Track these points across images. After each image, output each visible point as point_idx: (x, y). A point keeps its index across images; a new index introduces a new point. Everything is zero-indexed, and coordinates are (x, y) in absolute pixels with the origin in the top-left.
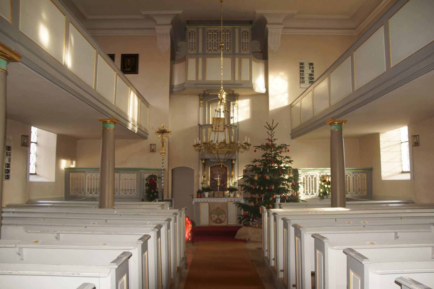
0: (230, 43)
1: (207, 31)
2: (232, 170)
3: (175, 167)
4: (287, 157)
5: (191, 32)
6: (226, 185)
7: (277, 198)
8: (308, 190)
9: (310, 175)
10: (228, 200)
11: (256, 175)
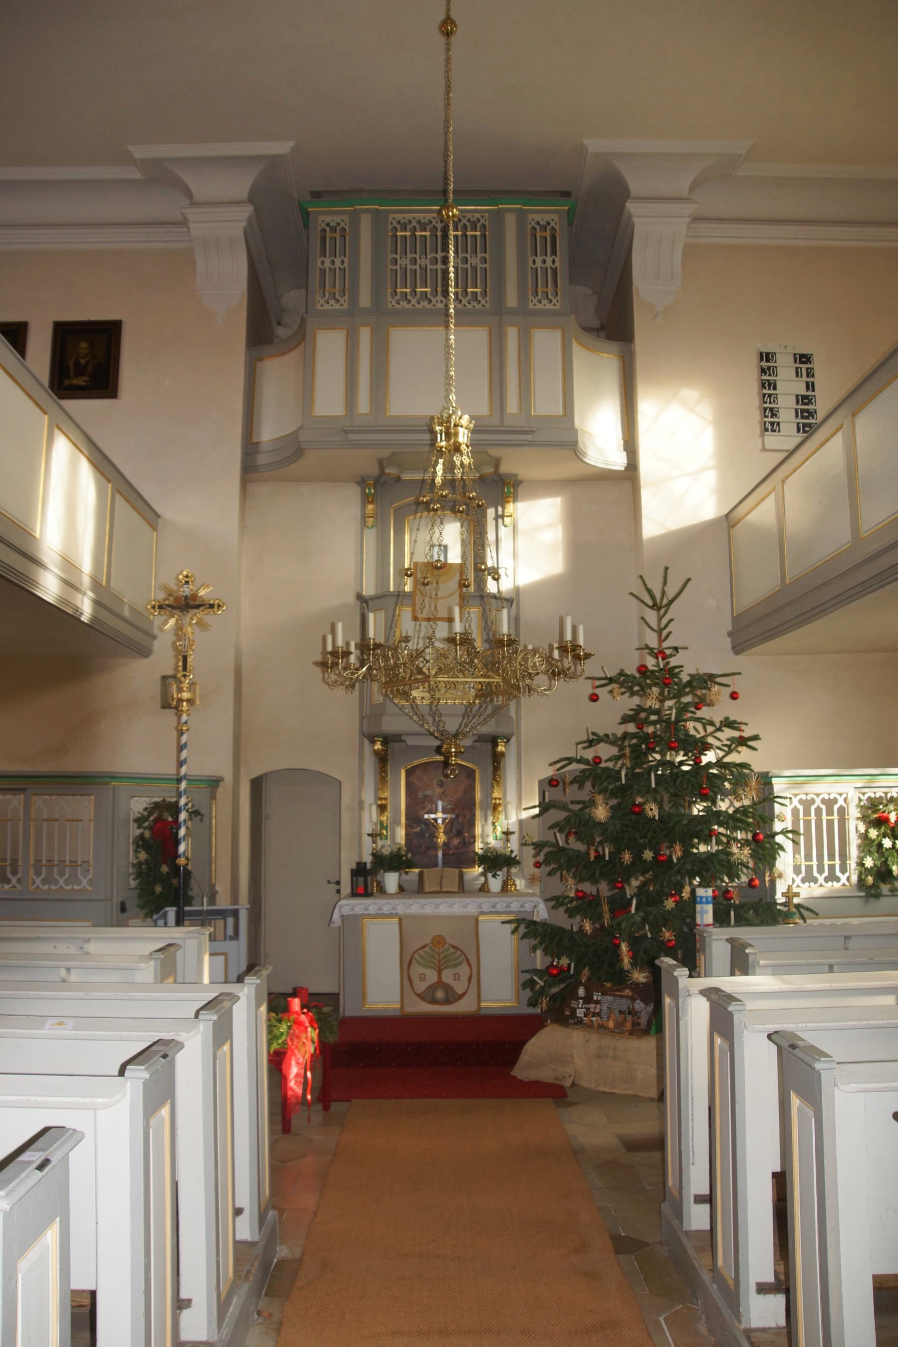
1: (392, 223)
2: (495, 779)
3: (268, 770)
4: (730, 724)
5: (328, 229)
6: (472, 840)
7: (701, 903)
8: (815, 863)
9: (821, 797)
11: (600, 799)
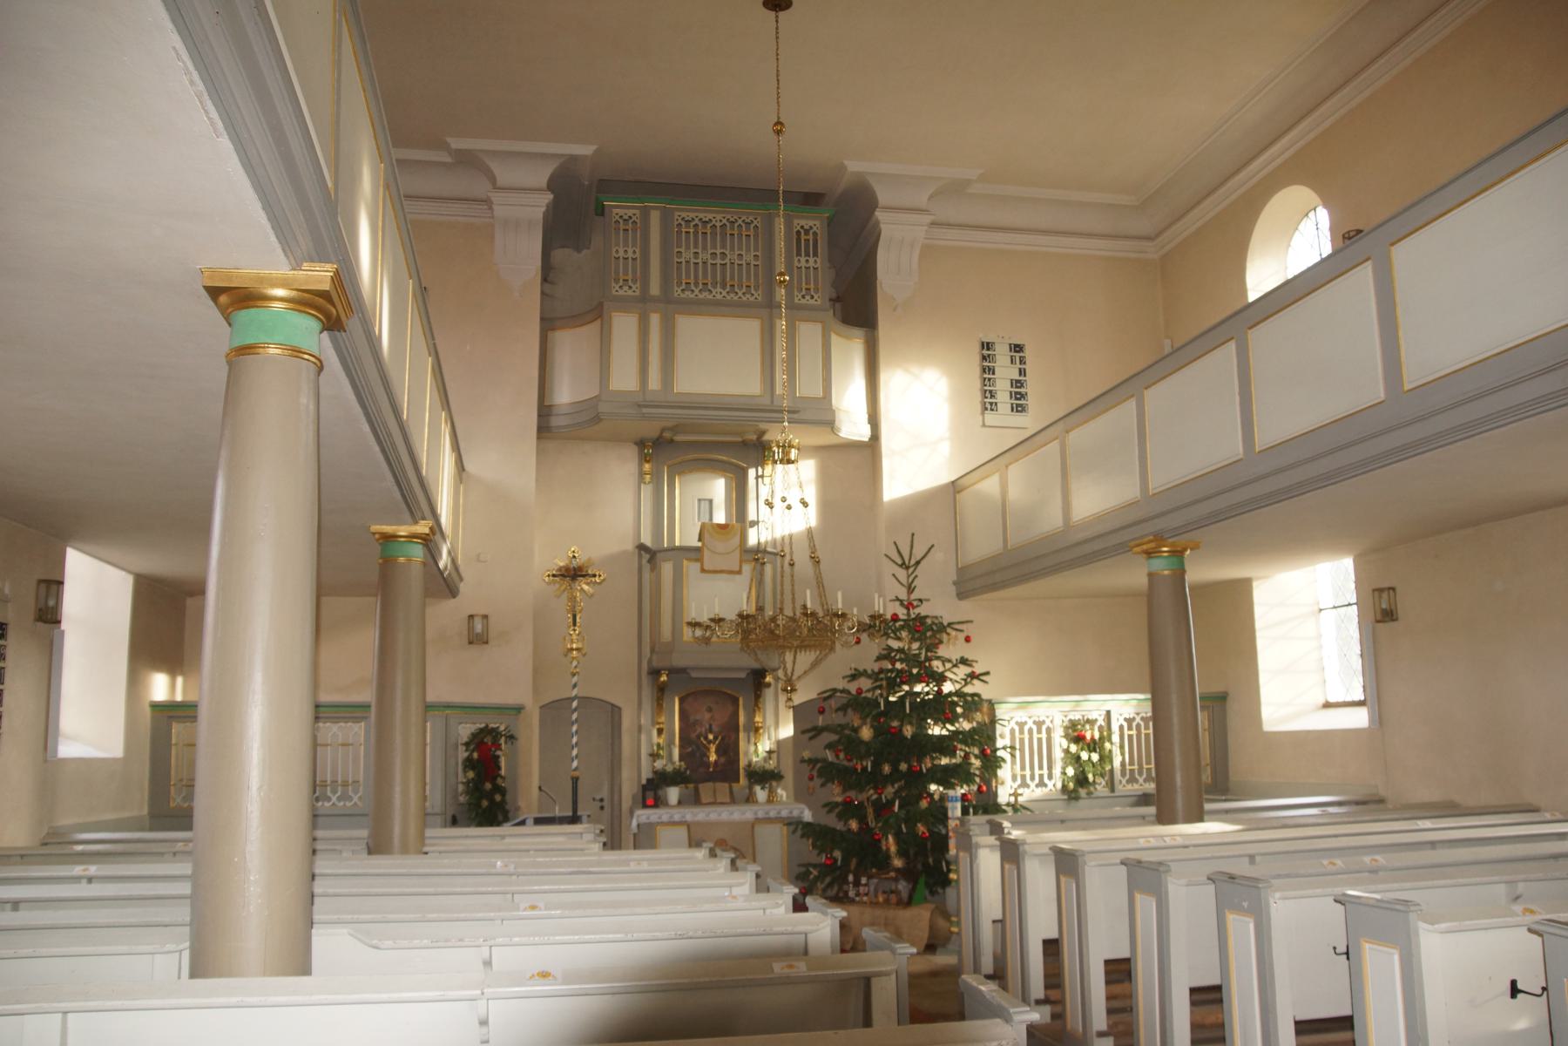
0: (758, 265)
4: (964, 661)
5: (621, 221)
7: (952, 801)
9: (1140, 716)
10: (756, 813)
